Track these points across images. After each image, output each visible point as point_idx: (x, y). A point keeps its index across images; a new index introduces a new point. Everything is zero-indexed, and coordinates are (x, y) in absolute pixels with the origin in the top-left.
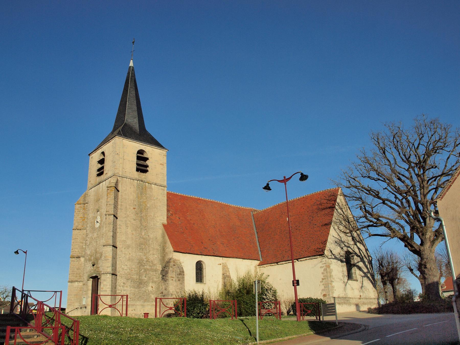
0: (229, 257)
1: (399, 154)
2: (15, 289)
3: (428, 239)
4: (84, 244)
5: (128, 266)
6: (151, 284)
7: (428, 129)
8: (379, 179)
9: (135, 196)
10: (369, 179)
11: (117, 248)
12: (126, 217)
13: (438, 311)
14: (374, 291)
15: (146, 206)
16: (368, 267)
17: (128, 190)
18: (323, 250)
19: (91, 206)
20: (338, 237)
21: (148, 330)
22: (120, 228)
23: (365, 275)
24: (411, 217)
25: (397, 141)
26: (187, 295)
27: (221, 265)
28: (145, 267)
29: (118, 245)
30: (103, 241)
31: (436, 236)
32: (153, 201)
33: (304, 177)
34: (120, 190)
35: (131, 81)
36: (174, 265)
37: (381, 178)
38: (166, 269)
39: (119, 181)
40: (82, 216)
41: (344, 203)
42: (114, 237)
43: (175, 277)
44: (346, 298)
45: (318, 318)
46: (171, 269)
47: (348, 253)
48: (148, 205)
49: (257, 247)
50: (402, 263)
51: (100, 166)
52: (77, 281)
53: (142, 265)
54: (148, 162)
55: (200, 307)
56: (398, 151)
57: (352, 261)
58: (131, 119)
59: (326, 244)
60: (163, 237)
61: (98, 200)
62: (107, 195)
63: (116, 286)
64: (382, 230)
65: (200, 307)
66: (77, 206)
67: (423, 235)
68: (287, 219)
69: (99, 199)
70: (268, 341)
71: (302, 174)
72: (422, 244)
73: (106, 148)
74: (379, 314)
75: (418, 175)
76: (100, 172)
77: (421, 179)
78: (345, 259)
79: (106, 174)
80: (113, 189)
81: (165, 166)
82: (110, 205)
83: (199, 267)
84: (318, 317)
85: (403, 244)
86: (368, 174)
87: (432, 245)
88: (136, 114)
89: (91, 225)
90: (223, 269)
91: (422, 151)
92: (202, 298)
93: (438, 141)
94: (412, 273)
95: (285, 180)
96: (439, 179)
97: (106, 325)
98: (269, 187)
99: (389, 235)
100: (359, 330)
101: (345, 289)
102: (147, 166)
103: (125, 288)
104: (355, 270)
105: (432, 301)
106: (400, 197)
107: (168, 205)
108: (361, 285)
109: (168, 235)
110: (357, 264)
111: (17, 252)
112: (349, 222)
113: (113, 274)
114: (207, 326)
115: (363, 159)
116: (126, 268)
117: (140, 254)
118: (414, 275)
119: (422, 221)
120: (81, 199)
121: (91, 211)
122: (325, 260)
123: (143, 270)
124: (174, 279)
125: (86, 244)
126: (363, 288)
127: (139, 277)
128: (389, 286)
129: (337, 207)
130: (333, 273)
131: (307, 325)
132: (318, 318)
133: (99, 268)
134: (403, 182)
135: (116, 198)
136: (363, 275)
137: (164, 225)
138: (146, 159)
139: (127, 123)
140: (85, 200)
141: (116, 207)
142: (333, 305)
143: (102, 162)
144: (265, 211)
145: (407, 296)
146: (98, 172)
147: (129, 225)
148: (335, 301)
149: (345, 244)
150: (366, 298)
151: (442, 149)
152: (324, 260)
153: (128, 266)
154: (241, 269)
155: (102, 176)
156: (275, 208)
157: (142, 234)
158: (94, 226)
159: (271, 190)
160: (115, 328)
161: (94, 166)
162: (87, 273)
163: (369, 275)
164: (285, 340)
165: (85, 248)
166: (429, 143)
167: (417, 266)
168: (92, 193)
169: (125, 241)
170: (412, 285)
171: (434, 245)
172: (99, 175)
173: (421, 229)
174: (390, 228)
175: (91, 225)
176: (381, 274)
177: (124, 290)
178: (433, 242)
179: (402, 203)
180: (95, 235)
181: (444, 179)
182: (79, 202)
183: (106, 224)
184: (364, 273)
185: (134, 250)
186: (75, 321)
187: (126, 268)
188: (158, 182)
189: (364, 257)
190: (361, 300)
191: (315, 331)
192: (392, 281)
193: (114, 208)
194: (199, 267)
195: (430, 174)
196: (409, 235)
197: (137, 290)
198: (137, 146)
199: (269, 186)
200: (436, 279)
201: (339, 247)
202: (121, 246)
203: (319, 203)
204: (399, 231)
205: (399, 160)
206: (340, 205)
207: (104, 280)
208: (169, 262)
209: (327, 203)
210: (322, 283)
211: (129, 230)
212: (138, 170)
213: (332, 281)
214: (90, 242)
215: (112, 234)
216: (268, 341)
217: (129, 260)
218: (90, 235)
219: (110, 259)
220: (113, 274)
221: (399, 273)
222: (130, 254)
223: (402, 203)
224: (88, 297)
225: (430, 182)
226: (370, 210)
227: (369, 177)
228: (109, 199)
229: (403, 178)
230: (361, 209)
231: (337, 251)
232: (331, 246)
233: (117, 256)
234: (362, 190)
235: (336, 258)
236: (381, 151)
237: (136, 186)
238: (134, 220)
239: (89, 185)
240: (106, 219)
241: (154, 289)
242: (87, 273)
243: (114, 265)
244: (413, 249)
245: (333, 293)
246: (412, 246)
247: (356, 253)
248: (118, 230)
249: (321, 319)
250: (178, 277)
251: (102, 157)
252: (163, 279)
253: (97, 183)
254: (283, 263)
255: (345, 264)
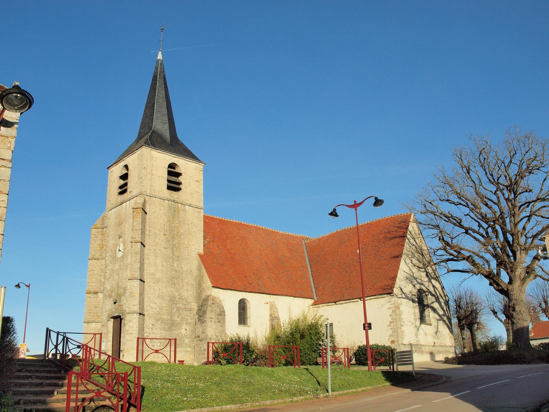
0: (278, 295)
1: (486, 173)
2: (50, 330)
3: (518, 277)
4: (103, 277)
5: (158, 304)
6: (184, 326)
7: (522, 145)
8: (460, 204)
9: (166, 220)
10: (447, 203)
11: (144, 282)
12: (155, 245)
13: (529, 363)
14: (450, 338)
15: (179, 231)
16: (445, 308)
17: (158, 212)
18: (392, 288)
19: (111, 231)
20: (409, 272)
21: (206, 378)
22: (148, 258)
23: (441, 318)
24: (499, 250)
25: (485, 159)
26: (228, 340)
27: (269, 304)
28: (178, 305)
29: (145, 278)
30: (128, 274)
31: (527, 273)
32: (187, 226)
33: (378, 202)
34: (147, 212)
35: (159, 81)
36: (213, 304)
37: (462, 202)
38: (203, 309)
39: (146, 201)
40: (99, 242)
41: (417, 231)
42: (142, 269)
43: (214, 317)
44: (417, 345)
45: (392, 368)
46: (209, 308)
47: (420, 291)
48: (181, 231)
49: (310, 283)
50: (484, 304)
51: (122, 182)
52: (94, 322)
53: (173, 303)
54: (181, 179)
55: (245, 353)
56: (485, 170)
57: (425, 301)
58: (160, 125)
59: (395, 280)
60: (199, 269)
61: (120, 224)
62: (133, 218)
63: (143, 328)
64: (464, 265)
65: (245, 353)
66: (94, 231)
67: (512, 271)
68: (358, 251)
69: (122, 223)
70: (341, 392)
71: (376, 198)
72: (511, 282)
73: (130, 160)
74: (459, 364)
75: (507, 200)
76: (123, 190)
77: (512, 205)
78: (417, 298)
79: (131, 192)
80: (141, 211)
81: (202, 183)
82: (136, 230)
83: (242, 306)
84: (392, 367)
85: (487, 282)
86: (446, 197)
87: (523, 284)
88: (166, 118)
89: (111, 254)
90: (271, 308)
91: (513, 170)
92: (247, 343)
93: (534, 160)
94: (496, 316)
95: (356, 206)
96: (533, 205)
97: (158, 372)
98: (336, 213)
99: (472, 271)
100: (440, 382)
101: (417, 336)
102: (180, 184)
103: (155, 331)
104: (429, 313)
105: (520, 349)
106: (485, 226)
107: (205, 231)
108: (435, 330)
109: (205, 267)
110: (432, 305)
111: (18, 286)
112: (422, 255)
113: (140, 314)
114: (271, 375)
115: (441, 179)
116: (155, 306)
117: (172, 289)
118: (499, 319)
119: (511, 254)
120: (99, 223)
121: (111, 237)
122: (393, 299)
123: (175, 309)
124: (213, 321)
125: (105, 277)
126: (438, 333)
127: (171, 317)
128: (467, 333)
129: (408, 236)
130: (403, 316)
131: (381, 375)
132: (392, 368)
133: (122, 306)
134: (490, 208)
135: (144, 222)
136: (438, 318)
137: (200, 255)
138: (178, 175)
139: (155, 129)
140: (103, 224)
141: (143, 233)
142: (410, 353)
143: (125, 177)
144: (319, 240)
145: (491, 343)
146: (120, 190)
147: (158, 255)
148: (411, 348)
149: (418, 280)
150: (442, 346)
151: (538, 169)
152: (393, 299)
153: (158, 304)
154: (293, 310)
155: (125, 195)
156: (332, 236)
157: (173, 266)
158: (116, 256)
159: (337, 216)
160: (169, 376)
161: (114, 182)
162: (106, 312)
163: (445, 318)
164: (358, 392)
165: (104, 282)
166: (523, 161)
167: (502, 308)
168: (112, 215)
169: (154, 274)
170: (494, 330)
171: (525, 284)
172: (121, 193)
173: (511, 265)
174: (474, 263)
175: (111, 254)
176: (458, 317)
177: (153, 333)
178: (523, 280)
179: (487, 233)
180: (117, 266)
181: (539, 205)
182: (97, 226)
183: (131, 253)
184: (439, 315)
185: (165, 285)
186: (135, 367)
187: (155, 306)
188: (194, 203)
189: (440, 297)
190: (436, 348)
191: (390, 381)
192: (470, 327)
193: (142, 234)
194: (242, 306)
195: (522, 198)
196: (495, 272)
197: (168, 333)
198: (168, 158)
199: (336, 211)
200: (525, 324)
201: (411, 285)
202: (149, 280)
203: (386, 231)
204: (483, 266)
205: (484, 179)
206: (413, 233)
207: (130, 321)
208: (207, 299)
209: (397, 231)
210: (390, 328)
211: (159, 261)
212: (169, 188)
213: (401, 325)
214: (111, 275)
215: (139, 266)
216: (341, 392)
217: (159, 297)
218: (110, 267)
219: (137, 296)
220: (140, 314)
221: (479, 316)
222: (160, 289)
223: (487, 233)
224: (109, 341)
225: (521, 209)
226: (449, 240)
227: (448, 200)
228: (135, 223)
229: (490, 203)
230: (439, 240)
231: (409, 289)
232: (402, 284)
233: (145, 292)
234: (441, 217)
235: (407, 297)
236: (465, 169)
237: (166, 208)
238: (165, 248)
239: (109, 205)
240: (132, 247)
241: (188, 332)
242: (106, 312)
243: (141, 303)
244: (500, 288)
245: (402, 339)
246: (498, 285)
247: (430, 292)
248: (146, 261)
249: (395, 370)
250: (218, 318)
251: (125, 172)
252: (199, 320)
253: (119, 203)
254: (343, 302)
255: (417, 304)
